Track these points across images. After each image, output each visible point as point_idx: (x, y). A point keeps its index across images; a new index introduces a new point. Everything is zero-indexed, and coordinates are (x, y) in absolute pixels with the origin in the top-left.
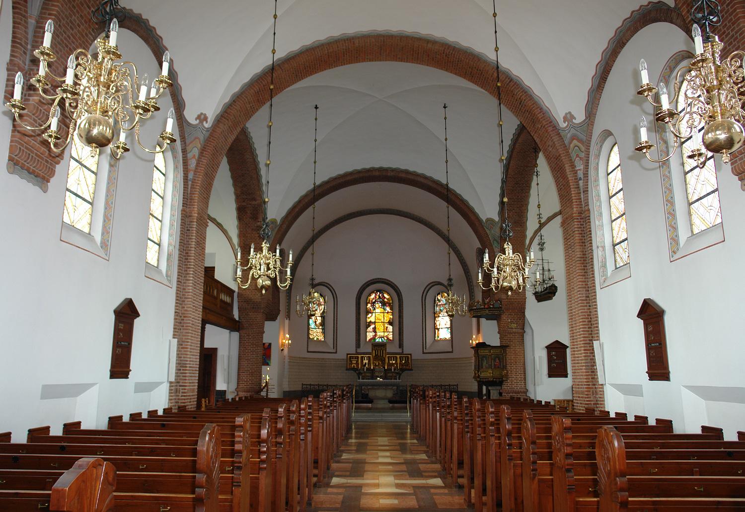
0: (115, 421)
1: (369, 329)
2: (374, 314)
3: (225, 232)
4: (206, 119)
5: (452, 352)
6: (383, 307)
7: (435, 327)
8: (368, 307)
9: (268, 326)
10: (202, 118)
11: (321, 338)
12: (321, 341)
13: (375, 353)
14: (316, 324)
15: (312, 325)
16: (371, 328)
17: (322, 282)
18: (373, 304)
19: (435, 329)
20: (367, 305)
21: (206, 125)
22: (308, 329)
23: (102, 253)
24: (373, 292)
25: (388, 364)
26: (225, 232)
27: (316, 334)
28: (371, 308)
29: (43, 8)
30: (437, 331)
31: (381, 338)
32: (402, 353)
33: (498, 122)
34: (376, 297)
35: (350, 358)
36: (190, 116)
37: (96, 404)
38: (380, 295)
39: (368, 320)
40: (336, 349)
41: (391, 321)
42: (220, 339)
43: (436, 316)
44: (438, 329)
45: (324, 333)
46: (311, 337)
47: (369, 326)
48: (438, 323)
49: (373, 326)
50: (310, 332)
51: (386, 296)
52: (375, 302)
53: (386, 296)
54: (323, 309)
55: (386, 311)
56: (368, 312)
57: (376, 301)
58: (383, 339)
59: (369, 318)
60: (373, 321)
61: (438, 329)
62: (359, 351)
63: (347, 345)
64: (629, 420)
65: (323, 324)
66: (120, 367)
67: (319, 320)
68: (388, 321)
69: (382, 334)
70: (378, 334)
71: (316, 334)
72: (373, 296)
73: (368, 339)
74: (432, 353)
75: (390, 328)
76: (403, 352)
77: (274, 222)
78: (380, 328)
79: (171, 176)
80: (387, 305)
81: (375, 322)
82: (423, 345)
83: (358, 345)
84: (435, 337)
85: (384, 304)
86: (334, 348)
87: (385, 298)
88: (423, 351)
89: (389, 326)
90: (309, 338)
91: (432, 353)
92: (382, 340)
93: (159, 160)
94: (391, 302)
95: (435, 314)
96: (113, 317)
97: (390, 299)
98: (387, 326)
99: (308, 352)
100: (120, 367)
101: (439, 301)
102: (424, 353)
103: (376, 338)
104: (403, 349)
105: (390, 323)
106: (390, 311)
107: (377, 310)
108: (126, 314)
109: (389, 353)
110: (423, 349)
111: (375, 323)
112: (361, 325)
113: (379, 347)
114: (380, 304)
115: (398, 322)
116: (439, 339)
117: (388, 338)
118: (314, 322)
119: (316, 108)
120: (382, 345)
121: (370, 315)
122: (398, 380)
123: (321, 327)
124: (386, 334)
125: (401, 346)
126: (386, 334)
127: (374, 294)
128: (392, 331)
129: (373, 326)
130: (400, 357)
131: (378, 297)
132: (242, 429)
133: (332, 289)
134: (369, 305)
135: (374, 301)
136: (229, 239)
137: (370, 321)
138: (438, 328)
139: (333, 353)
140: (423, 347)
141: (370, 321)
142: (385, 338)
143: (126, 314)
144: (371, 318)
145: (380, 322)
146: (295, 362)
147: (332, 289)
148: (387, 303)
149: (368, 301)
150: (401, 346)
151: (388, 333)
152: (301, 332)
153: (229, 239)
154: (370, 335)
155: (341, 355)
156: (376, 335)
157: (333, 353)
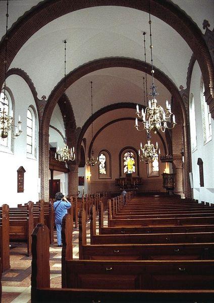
0: (19, 206)
3: (58, 131)
4: (45, 97)
10: (44, 97)
11: (105, 173)
16: (125, 168)
21: (46, 100)
22: (99, 169)
23: (12, 153)
26: (58, 131)
27: (103, 171)
35: (117, 180)
36: (40, 97)
37: (14, 200)
42: (62, 178)
49: (126, 167)
53: (132, 154)
56: (124, 161)
63: (115, 176)
64: (199, 203)
65: (105, 167)
66: (20, 189)
67: (104, 165)
71: (103, 171)
72: (126, 154)
75: (134, 167)
77: (79, 128)
78: (129, 167)
79: (34, 120)
83: (120, 175)
85: (131, 157)
90: (99, 173)
93: (29, 114)
96: (17, 173)
100: (20, 189)
105: (134, 165)
108: (21, 171)
112: (121, 166)
119: (92, 83)
120: (131, 174)
125: (138, 174)
136: (62, 136)
143: (21, 171)
144: (125, 163)
146: (93, 184)
150: (138, 174)
152: (95, 168)
153: (62, 136)
154: (125, 171)
155: (113, 179)
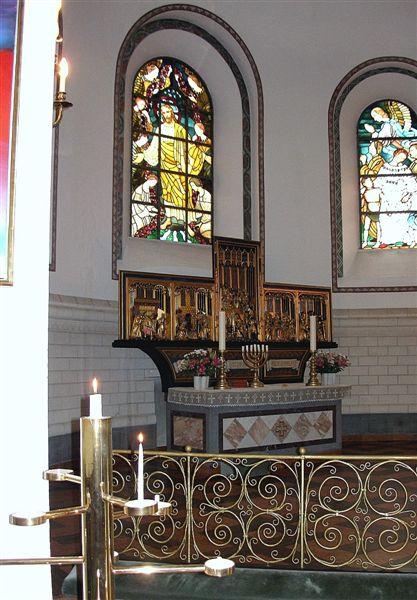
1: (139, 190)
2: (156, 138)
6: (183, 121)
8: (136, 109)
16: (143, 191)
17: (153, 12)
18: (154, 102)
19: (361, 213)
24: (153, 62)
28: (145, 113)
30: (367, 220)
34: (162, 81)
43: (362, 172)
44: (375, 216)
47: (141, 181)
48: (371, 196)
49: (151, 183)
51: (192, 82)
53: (192, 82)
55: (195, 138)
59: (139, 150)
60: (153, 162)
61: (375, 216)
68: (197, 173)
69: (180, 215)
70: (169, 212)
72: (153, 74)
74: (368, 290)
84: (361, 242)
87: (190, 89)
89: (201, 190)
91: (368, 290)
92: (179, 236)
95: (360, 166)
97: (206, 98)
98: (196, 188)
101: (378, 126)
103: (163, 227)
106: (204, 138)
109: (266, 285)
111: (157, 171)
116: (377, 245)
121: (142, 141)
124: (192, 217)
126: (192, 217)
127: (156, 70)
128: (207, 207)
129: (151, 183)
131: (168, 82)
132: (294, 364)
134: (141, 104)
137: (144, 162)
138: (373, 208)
141: (144, 162)
142: (191, 233)
147: (366, 69)
149: (136, 88)
151: (199, 215)
156: (160, 217)
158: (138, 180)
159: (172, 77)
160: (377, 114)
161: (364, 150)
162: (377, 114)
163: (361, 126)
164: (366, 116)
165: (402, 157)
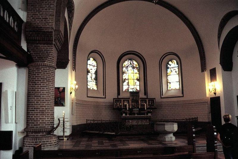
5: (183, 96)
7: (167, 81)
9: (59, 73)
11: (95, 88)
12: (95, 90)
13: (132, 98)
14: (91, 78)
15: (89, 79)
16: (125, 83)
17: (93, 51)
20: (123, 69)
25: (141, 105)
29: (29, 74)
30: (169, 84)
31: (132, 89)
32: (147, 98)
33: (154, 4)
38: (131, 62)
39: (124, 78)
40: (105, 95)
41: (138, 78)
43: (168, 75)
44: (170, 83)
45: (97, 84)
46: (89, 87)
49: (127, 81)
50: (88, 84)
52: (127, 67)
54: (96, 69)
56: (123, 73)
57: (128, 66)
58: (133, 89)
62: (119, 97)
65: (96, 79)
67: (94, 76)
71: (92, 85)
73: (124, 90)
75: (138, 83)
76: (147, 97)
78: (131, 82)
80: (136, 68)
81: (128, 79)
82: (161, 93)
83: (119, 94)
85: (133, 68)
86: (104, 95)
88: (161, 97)
94: (138, 66)
99: (88, 97)
102: (161, 98)
104: (147, 96)
107: (129, 72)
110: (161, 96)
112: (119, 81)
113: (135, 94)
114: (131, 68)
115: (144, 79)
117: (136, 89)
118: (91, 76)
122: (146, 115)
123: (95, 81)
124: (135, 86)
125: (146, 93)
130: (123, 101)
131: (129, 63)
133: (102, 57)
135: (127, 66)
137: (125, 78)
139: (103, 98)
140: (161, 94)
144: (125, 76)
145: (131, 79)
148: (136, 67)
154: (125, 87)
157: (103, 98)
158: (125, 81)
159: (130, 62)
160: (170, 63)
161: (168, 70)
162: (170, 63)
163: (167, 66)
164: (168, 63)
165: (175, 71)
